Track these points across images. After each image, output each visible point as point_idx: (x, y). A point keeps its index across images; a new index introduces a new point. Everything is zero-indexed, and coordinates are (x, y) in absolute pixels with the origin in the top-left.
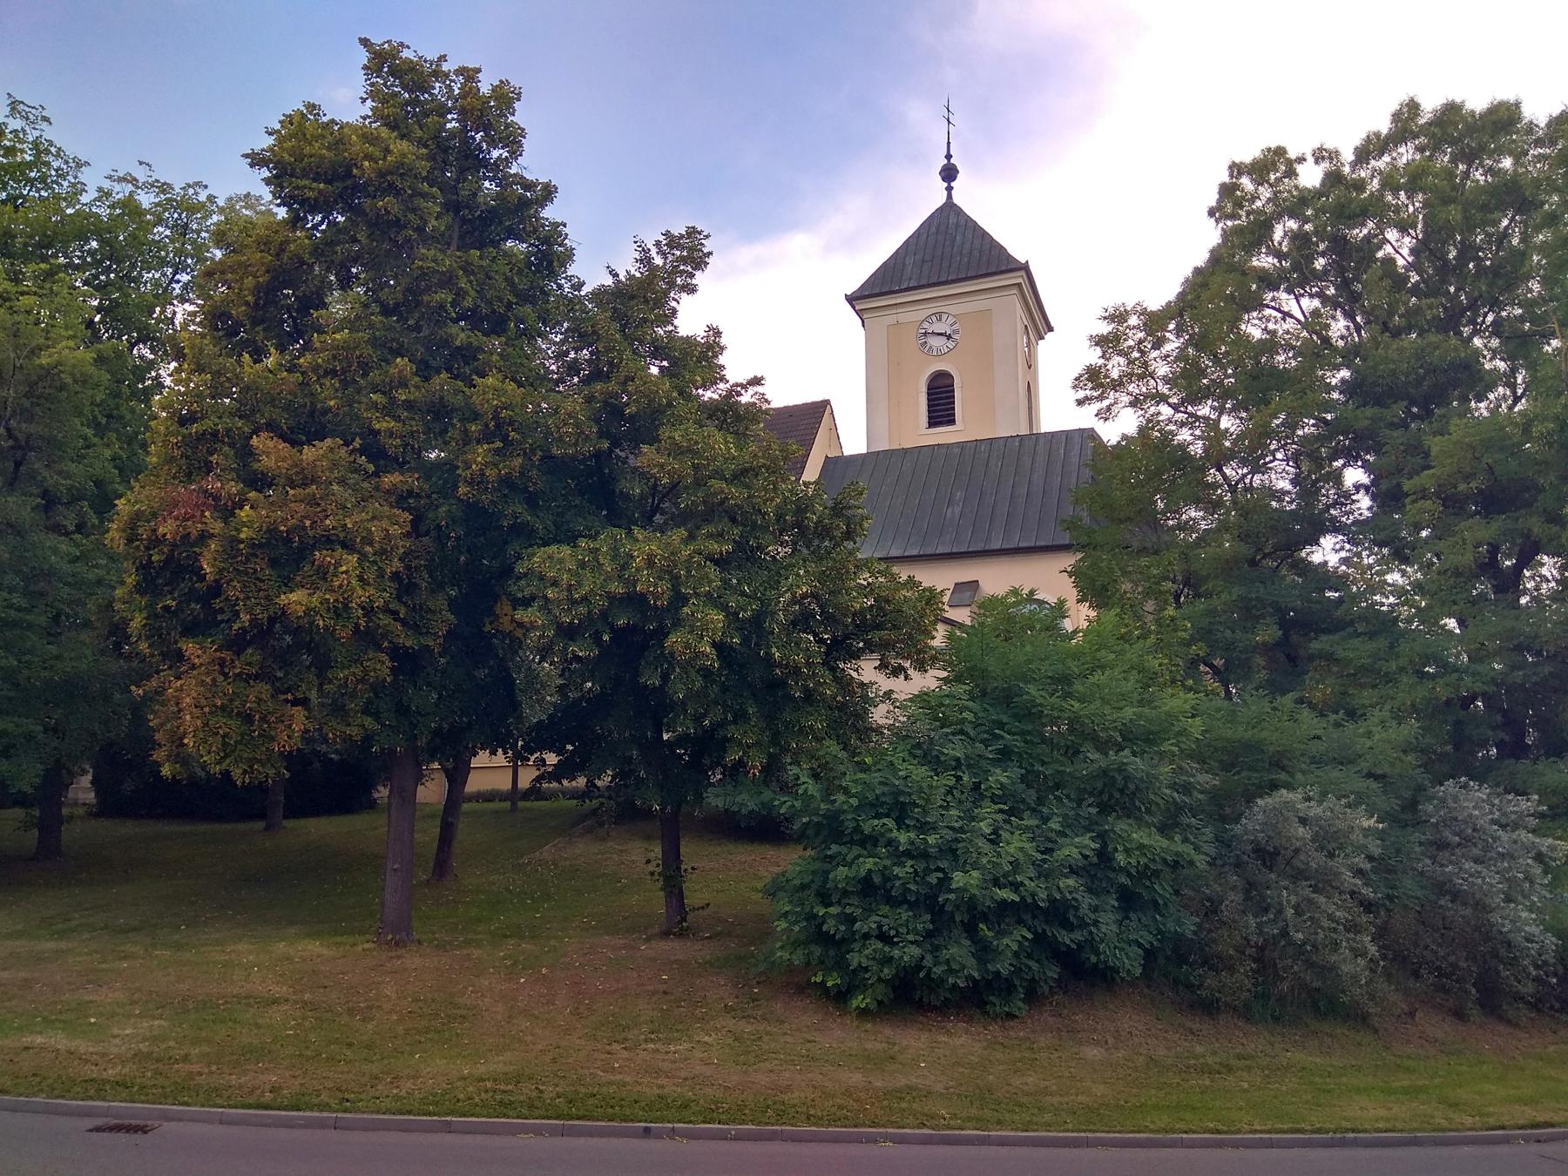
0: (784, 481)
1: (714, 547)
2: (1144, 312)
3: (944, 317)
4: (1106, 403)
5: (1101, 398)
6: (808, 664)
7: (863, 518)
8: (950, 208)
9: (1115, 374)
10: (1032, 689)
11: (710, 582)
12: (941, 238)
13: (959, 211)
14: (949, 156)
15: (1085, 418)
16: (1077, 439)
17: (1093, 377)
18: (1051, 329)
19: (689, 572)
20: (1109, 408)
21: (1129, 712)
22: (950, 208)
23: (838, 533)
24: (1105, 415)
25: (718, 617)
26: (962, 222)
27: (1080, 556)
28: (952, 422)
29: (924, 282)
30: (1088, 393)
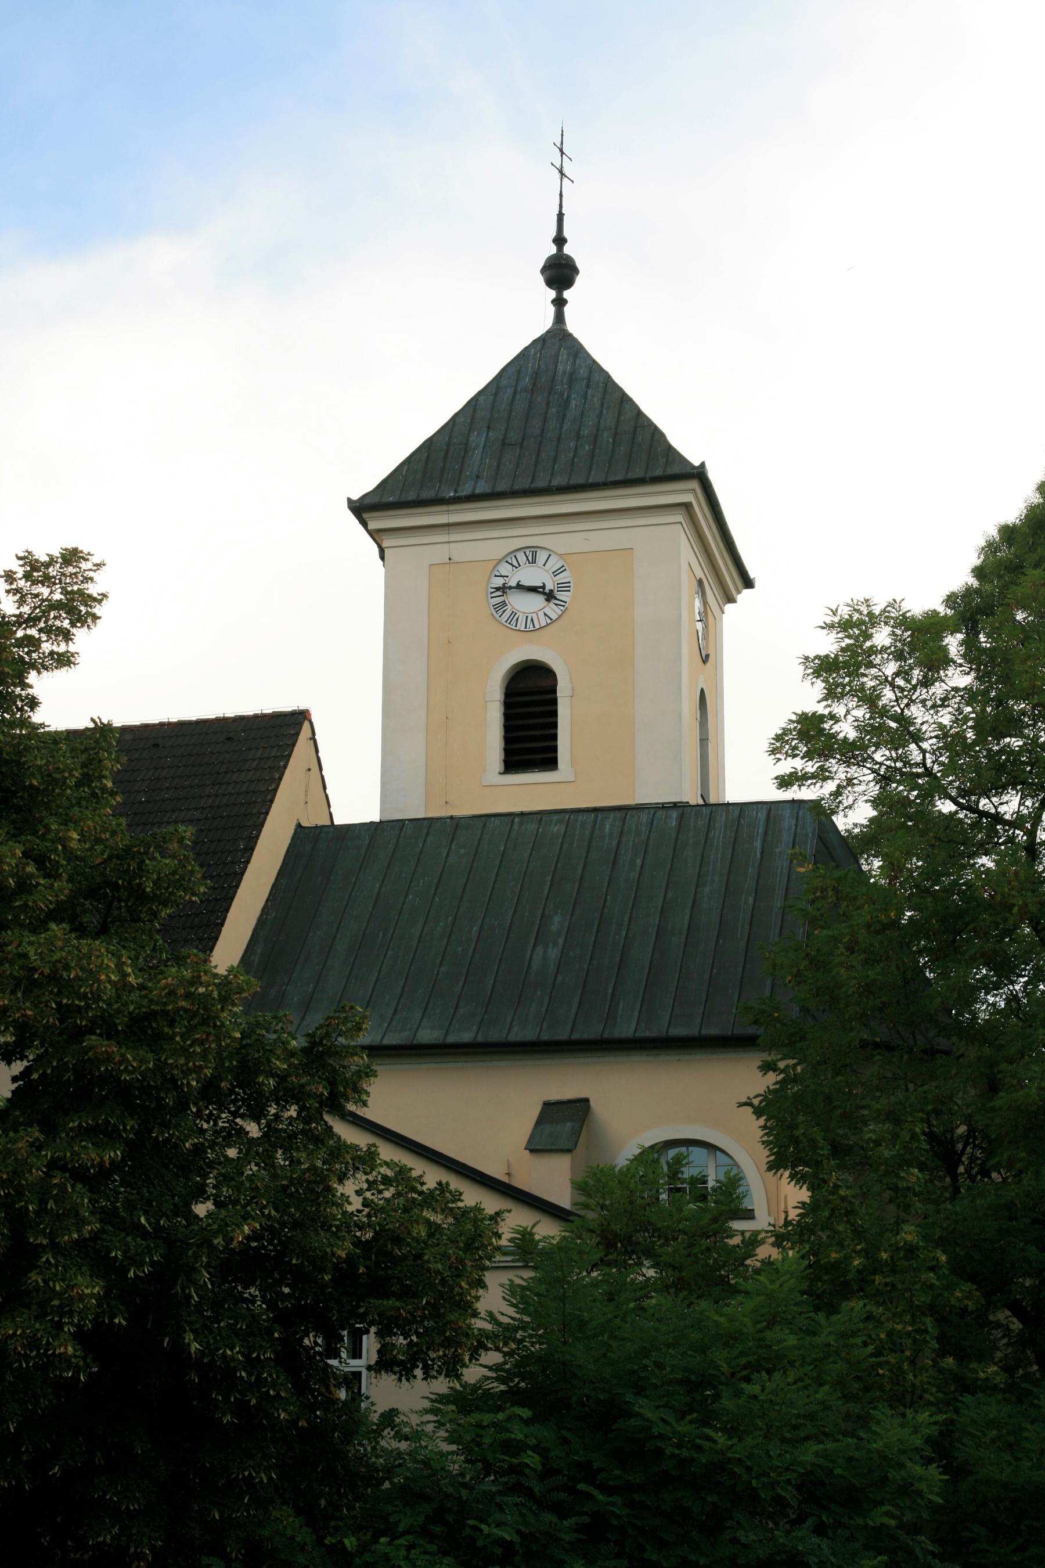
1: (91, 1155)
2: (904, 622)
3: (542, 556)
6: (251, 1364)
8: (558, 341)
10: (645, 1408)
11: (82, 1222)
12: (540, 399)
13: (576, 350)
14: (560, 240)
17: (810, 734)
18: (748, 583)
19: (42, 1202)
21: (809, 1454)
22: (558, 341)
25: (90, 1288)
26: (583, 372)
28: (550, 762)
29: (502, 486)
30: (798, 764)
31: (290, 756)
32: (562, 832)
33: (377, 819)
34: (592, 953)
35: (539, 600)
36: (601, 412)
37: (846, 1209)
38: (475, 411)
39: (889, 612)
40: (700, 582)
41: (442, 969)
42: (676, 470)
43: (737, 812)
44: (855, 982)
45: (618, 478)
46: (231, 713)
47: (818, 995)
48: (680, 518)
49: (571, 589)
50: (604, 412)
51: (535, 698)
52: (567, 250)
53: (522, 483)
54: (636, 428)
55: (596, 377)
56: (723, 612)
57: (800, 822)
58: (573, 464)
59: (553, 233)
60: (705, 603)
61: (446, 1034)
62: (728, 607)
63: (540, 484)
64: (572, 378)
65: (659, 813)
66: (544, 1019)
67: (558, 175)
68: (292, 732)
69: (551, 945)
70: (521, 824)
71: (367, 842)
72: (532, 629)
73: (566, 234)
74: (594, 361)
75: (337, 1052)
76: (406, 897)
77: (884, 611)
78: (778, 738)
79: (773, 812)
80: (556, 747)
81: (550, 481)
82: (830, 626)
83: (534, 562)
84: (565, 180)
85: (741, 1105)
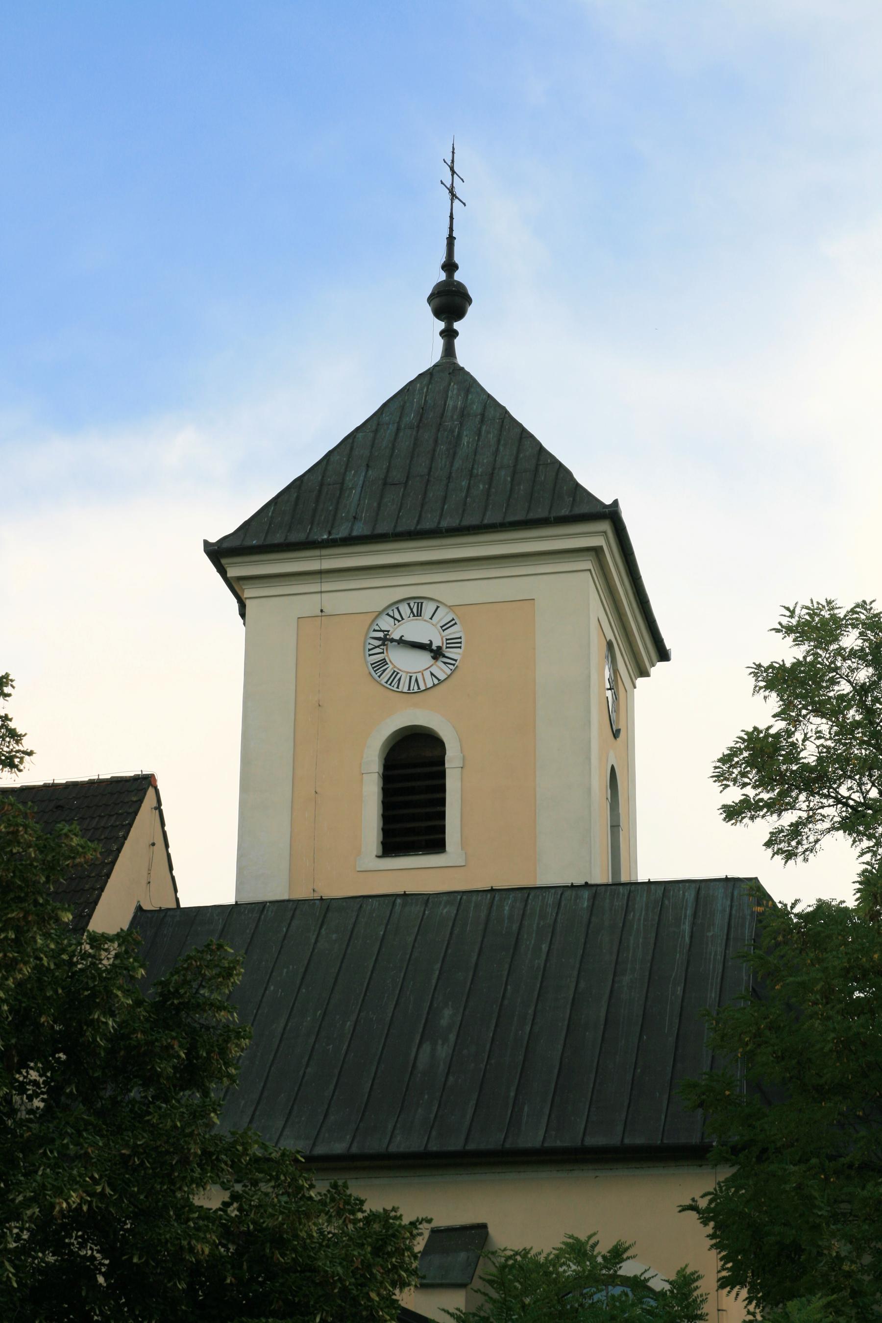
0: (42, 921)
4: (789, 818)
5: (776, 807)
7: (230, 1034)
8: (448, 374)
9: (809, 754)
13: (468, 384)
14: (450, 266)
15: (738, 852)
16: (721, 902)
17: (762, 762)
18: (663, 655)
20: (796, 830)
22: (448, 374)
23: (165, 1068)
24: (788, 844)
27: (726, 1172)
28: (437, 845)
30: (750, 792)
31: (130, 825)
32: (453, 915)
33: (231, 900)
34: (490, 1051)
35: (423, 659)
36: (497, 449)
37: (852, 1289)
38: (352, 449)
39: (857, 613)
40: (610, 645)
41: (309, 1070)
42: (584, 509)
43: (660, 892)
44: (833, 1035)
45: (517, 518)
46: (61, 779)
47: (783, 1058)
48: (588, 565)
49: (462, 645)
50: (501, 448)
51: (418, 770)
52: (458, 276)
53: (408, 523)
54: (537, 465)
55: (491, 413)
56: (635, 687)
57: (736, 903)
58: (465, 504)
59: (442, 258)
60: (615, 671)
61: (314, 1145)
62: (640, 681)
63: (427, 525)
64: (463, 414)
65: (568, 893)
66: (432, 1128)
67: (448, 196)
68: (134, 799)
69: (440, 1042)
70: (404, 905)
71: (220, 927)
72: (416, 691)
73: (457, 259)
74: (489, 396)
75: (198, 1005)
76: (266, 989)
77: (853, 611)
78: (725, 759)
79: (703, 892)
80: (444, 826)
81: (439, 523)
82: (789, 630)
83: (419, 614)
84: (456, 201)
85: (684, 1209)
